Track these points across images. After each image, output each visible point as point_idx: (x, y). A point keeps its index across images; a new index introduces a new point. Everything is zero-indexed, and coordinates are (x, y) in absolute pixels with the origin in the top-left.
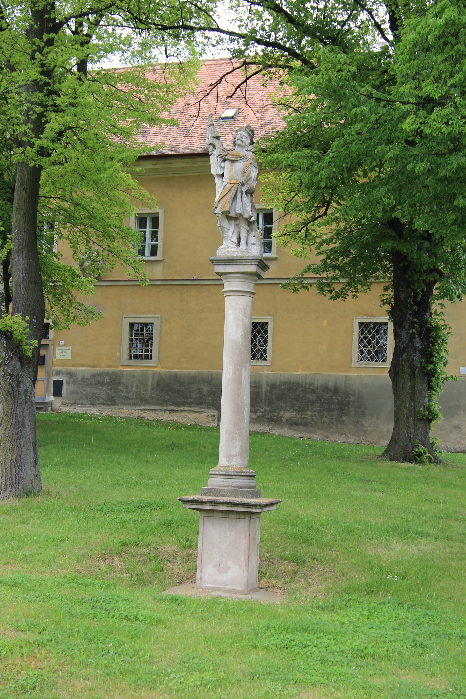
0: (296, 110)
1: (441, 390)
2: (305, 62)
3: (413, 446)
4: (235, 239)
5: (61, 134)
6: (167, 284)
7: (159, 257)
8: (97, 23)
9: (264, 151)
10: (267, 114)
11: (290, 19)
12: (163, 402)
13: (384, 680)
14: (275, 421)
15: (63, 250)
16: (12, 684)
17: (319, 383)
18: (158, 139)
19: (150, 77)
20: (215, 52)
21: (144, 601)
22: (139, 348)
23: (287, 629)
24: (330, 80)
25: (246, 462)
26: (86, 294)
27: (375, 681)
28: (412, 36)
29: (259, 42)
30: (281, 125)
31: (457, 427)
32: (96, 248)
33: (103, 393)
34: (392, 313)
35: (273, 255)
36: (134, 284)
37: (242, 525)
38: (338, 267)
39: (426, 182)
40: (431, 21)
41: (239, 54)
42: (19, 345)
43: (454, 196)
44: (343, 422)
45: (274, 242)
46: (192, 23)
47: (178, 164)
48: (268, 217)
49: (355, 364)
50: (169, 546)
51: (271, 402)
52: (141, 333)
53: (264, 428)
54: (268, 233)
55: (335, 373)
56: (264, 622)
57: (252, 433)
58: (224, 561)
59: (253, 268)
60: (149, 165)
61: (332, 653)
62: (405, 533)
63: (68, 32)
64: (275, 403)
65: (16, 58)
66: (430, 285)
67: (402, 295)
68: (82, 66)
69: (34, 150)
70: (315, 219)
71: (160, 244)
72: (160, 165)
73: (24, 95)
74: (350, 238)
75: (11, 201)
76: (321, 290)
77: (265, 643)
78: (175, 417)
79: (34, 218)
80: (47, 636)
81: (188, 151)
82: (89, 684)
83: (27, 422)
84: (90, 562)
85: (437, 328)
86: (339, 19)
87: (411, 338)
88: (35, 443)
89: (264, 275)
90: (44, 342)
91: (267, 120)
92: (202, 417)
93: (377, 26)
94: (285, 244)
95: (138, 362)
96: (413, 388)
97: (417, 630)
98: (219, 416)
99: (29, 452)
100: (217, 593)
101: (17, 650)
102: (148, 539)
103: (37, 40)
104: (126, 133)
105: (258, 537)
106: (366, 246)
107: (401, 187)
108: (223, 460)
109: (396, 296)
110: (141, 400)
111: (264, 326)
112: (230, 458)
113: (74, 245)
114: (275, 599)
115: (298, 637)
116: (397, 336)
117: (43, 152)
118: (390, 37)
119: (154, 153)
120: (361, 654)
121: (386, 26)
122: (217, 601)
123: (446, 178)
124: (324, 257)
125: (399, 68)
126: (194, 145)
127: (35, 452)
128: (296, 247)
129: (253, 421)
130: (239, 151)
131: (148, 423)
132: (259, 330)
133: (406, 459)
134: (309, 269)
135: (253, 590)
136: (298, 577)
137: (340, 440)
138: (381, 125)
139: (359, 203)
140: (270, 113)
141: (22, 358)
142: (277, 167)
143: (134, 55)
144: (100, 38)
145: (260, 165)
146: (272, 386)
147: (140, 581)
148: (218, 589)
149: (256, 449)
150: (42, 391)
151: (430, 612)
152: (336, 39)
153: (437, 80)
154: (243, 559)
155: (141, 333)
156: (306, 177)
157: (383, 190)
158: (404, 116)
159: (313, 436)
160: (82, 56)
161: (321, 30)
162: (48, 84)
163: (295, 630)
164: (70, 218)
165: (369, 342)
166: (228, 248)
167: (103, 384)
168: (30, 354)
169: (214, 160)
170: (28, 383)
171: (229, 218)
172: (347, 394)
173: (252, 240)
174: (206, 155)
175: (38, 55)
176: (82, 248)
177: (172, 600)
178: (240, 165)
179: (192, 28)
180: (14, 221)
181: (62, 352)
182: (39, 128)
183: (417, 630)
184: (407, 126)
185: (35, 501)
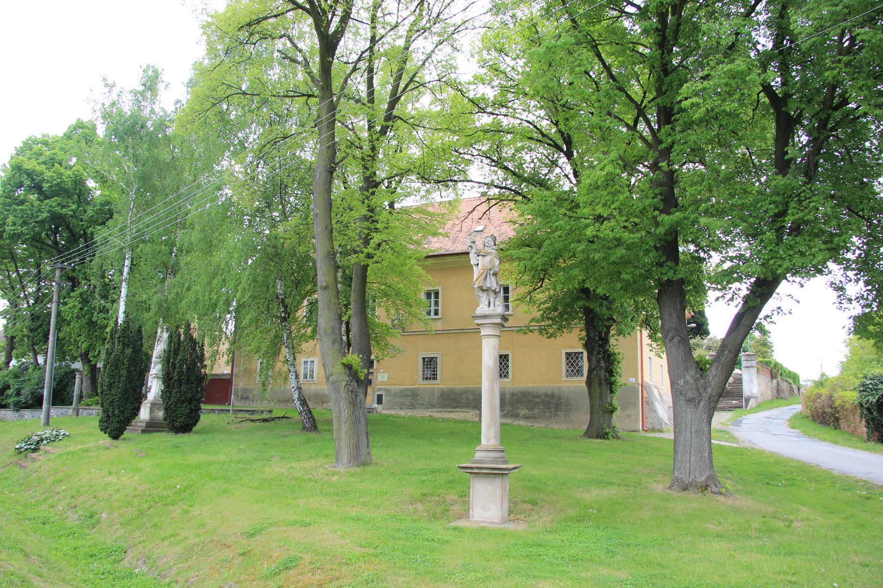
0: (521, 225)
1: (618, 393)
2: (524, 197)
3: (602, 428)
4: (487, 303)
5: (379, 245)
6: (445, 333)
7: (440, 316)
8: (400, 182)
9: (502, 250)
10: (503, 228)
11: (514, 174)
12: (445, 406)
13: (589, 574)
14: (516, 416)
15: (381, 314)
16: (360, 578)
17: (542, 392)
18: (437, 245)
19: (430, 209)
20: (469, 193)
21: (438, 529)
22: (429, 373)
23: (528, 545)
24: (540, 206)
25: (498, 442)
26: (396, 340)
27: (584, 575)
28: (588, 181)
29: (496, 187)
30: (512, 234)
31: (629, 416)
32: (401, 312)
33: (408, 401)
34: (586, 346)
35: (510, 312)
36: (424, 333)
37: (498, 481)
38: (551, 318)
39: (603, 265)
40: (598, 173)
41: (484, 194)
42: (356, 373)
43: (620, 273)
44: (558, 415)
45: (511, 304)
46: (455, 178)
47: (450, 259)
48: (506, 290)
49: (564, 378)
50: (452, 496)
51: (512, 404)
52: (430, 363)
53: (508, 421)
54: (506, 299)
55: (551, 385)
56: (513, 541)
57: (502, 425)
58: (487, 504)
59: (499, 321)
60: (432, 261)
61: (557, 559)
62: (600, 483)
63: (383, 187)
64: (515, 404)
65: (354, 203)
66: (608, 328)
67: (592, 334)
68: (391, 205)
69: (364, 255)
70: (535, 290)
71: (440, 308)
72: (439, 260)
73: (358, 224)
74: (557, 301)
75: (350, 286)
76: (541, 333)
77: (515, 554)
78: (452, 415)
79: (364, 296)
80: (379, 551)
81: (456, 252)
82: (406, 579)
83: (362, 420)
84: (403, 506)
85: (614, 354)
86: (543, 172)
87: (598, 361)
88: (367, 433)
89: (506, 325)
90: (371, 371)
91: (503, 231)
92: (470, 415)
93: (566, 176)
94: (517, 306)
95: (428, 382)
96: (601, 393)
97: (609, 543)
98: (480, 414)
99: (363, 438)
100: (483, 524)
101: (361, 559)
102: (438, 492)
103: (366, 193)
104: (418, 243)
105: (508, 489)
106: (568, 305)
107: (587, 268)
108: (484, 441)
109: (588, 335)
110: (431, 406)
111: (506, 356)
112: (488, 440)
113: (388, 311)
114: (520, 527)
115: (534, 550)
116: (589, 360)
117: (369, 256)
118: (574, 182)
119: (435, 253)
120: (574, 559)
121: (571, 176)
122: (483, 529)
123: (614, 262)
124: (542, 312)
125: (581, 199)
126: (460, 248)
127: (367, 438)
128: (524, 307)
129: (502, 417)
130: (489, 250)
131: (436, 420)
132: (503, 359)
133: (598, 437)
134: (533, 319)
135: (505, 522)
136: (533, 513)
137: (556, 427)
138: (573, 232)
139: (563, 279)
140: (506, 227)
141: (358, 381)
142: (511, 259)
143: (422, 197)
144: (402, 189)
145: (500, 258)
146: (513, 394)
147: (436, 517)
148: (483, 522)
149: (504, 434)
150: (370, 401)
151: (616, 531)
152: (542, 184)
153: (605, 205)
154: (498, 502)
155: (430, 363)
156: (529, 264)
157: (577, 270)
158: (587, 226)
159: (540, 425)
160: (391, 199)
161: (533, 179)
162: (371, 217)
163: (533, 545)
164: (386, 295)
165: (572, 364)
166: (482, 308)
167: (407, 396)
168: (362, 378)
169: (472, 256)
170: (362, 396)
171: (483, 290)
172: (560, 398)
173: (498, 303)
174: (468, 253)
175: (366, 201)
176: (393, 312)
177: (455, 529)
178: (488, 258)
179: (456, 181)
180: (352, 299)
181: (381, 377)
182: (366, 242)
183: (609, 543)
184: (590, 232)
185: (369, 469)
